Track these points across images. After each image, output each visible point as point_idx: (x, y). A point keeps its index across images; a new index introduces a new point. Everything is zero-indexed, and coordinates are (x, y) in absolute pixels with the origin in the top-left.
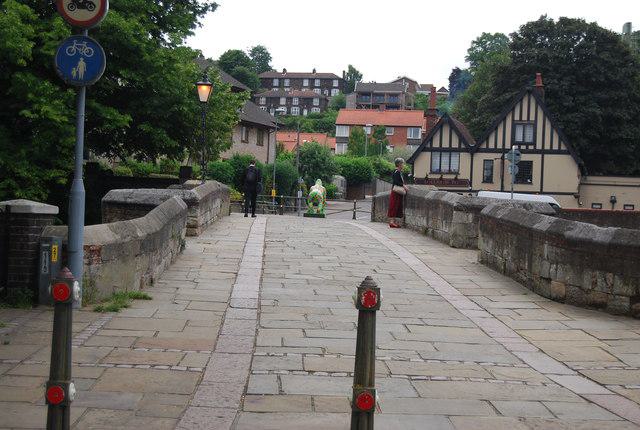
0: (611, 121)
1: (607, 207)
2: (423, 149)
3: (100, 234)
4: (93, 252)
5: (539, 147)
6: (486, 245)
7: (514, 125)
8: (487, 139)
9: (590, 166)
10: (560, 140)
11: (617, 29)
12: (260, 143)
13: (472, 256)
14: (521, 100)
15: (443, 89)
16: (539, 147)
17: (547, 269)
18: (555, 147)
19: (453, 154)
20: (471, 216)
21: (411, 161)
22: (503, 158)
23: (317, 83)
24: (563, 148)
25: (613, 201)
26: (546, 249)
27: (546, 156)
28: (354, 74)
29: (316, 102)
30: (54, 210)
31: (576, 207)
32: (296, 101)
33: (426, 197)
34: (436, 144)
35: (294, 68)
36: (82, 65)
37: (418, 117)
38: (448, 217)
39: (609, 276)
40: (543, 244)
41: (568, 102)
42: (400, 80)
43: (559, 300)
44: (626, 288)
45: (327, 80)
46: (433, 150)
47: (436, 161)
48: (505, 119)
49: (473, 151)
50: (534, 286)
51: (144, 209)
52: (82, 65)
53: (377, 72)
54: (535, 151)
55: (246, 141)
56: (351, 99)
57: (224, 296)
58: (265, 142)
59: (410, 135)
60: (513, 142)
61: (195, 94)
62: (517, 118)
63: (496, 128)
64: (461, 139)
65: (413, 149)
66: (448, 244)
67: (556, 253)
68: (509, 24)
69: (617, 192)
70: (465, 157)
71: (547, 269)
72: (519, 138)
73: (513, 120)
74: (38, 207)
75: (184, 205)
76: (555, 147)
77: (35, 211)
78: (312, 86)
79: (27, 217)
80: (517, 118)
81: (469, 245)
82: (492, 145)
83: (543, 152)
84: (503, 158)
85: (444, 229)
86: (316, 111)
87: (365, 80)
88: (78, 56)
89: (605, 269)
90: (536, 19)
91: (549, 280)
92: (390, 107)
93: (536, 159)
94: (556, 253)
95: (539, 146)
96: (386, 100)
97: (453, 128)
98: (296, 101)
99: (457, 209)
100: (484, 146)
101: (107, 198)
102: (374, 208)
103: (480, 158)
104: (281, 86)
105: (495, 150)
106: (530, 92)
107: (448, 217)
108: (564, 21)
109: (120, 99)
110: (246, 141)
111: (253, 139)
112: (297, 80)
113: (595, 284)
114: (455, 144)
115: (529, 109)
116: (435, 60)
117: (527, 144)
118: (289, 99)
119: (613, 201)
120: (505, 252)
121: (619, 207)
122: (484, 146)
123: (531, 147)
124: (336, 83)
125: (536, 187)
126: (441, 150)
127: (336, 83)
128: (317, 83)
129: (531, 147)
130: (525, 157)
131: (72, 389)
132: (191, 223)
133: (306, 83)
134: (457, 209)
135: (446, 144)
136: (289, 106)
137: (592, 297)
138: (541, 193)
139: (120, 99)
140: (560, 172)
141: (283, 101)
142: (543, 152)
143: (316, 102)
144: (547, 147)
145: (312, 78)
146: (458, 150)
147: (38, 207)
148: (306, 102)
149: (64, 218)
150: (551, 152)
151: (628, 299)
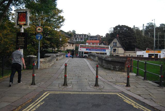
0: (130, 42)
1: (128, 56)
3: (42, 60)
4: (41, 62)
5: (117, 46)
11: (132, 27)
12: (73, 46)
14: (114, 39)
15: (105, 37)
16: (117, 46)
17: (104, 64)
18: (120, 46)
23: (83, 36)
29: (83, 39)
30: (36, 57)
31: (124, 56)
32: (80, 39)
35: (79, 33)
36: (39, 37)
41: (123, 39)
42: (97, 35)
43: (105, 68)
48: (112, 42)
50: (114, 69)
51: (49, 56)
52: (39, 37)
53: (93, 34)
54: (116, 47)
57: (59, 68)
60: (113, 46)
61: (59, 39)
62: (114, 42)
68: (123, 25)
69: (130, 54)
71: (104, 64)
72: (114, 45)
74: (34, 56)
75: (55, 56)
76: (120, 46)
77: (33, 57)
78: (83, 36)
79: (32, 58)
80: (114, 42)
83: (118, 47)
86: (83, 41)
88: (39, 36)
89: (110, 64)
90: (118, 25)
92: (95, 40)
93: (117, 48)
96: (95, 39)
98: (80, 39)
101: (45, 55)
104: (77, 36)
106: (116, 38)
108: (122, 26)
109: (48, 39)
112: (80, 35)
113: (109, 66)
115: (115, 40)
116: (103, 31)
118: (79, 39)
119: (129, 55)
121: (130, 56)
124: (86, 36)
125: (117, 53)
127: (86, 36)
131: (35, 75)
133: (81, 36)
138: (118, 54)
139: (48, 39)
141: (78, 39)
142: (118, 47)
143: (83, 39)
144: (119, 46)
145: (82, 35)
147: (34, 56)
148: (82, 39)
149: (37, 58)
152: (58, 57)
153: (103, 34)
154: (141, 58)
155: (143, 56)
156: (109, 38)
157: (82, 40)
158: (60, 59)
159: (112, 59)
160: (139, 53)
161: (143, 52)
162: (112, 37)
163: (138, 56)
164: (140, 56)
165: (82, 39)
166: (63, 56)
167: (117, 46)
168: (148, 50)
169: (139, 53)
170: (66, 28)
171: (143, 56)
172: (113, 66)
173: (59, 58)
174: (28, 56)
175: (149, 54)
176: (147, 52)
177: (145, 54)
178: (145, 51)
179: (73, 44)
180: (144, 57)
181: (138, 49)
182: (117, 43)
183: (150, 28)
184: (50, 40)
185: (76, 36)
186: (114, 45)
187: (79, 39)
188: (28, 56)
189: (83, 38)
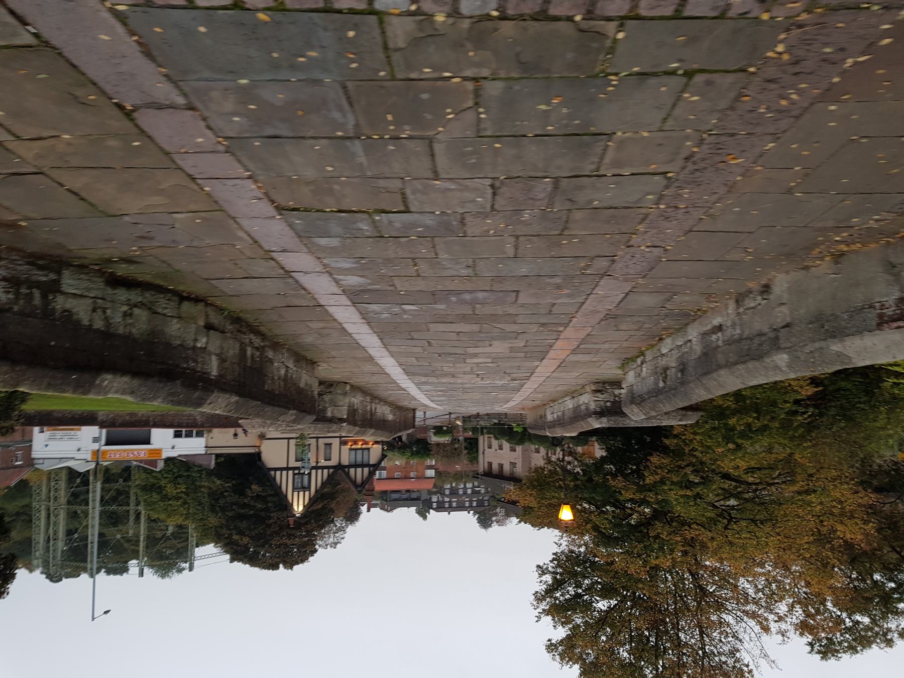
2: (376, 467)
6: (306, 379)
7: (309, 488)
8: (329, 476)
9: (255, 459)
10: (275, 479)
12: (490, 464)
13: (324, 371)
18: (278, 473)
19: (353, 463)
20: (329, 414)
21: (384, 456)
22: (317, 462)
23: (447, 505)
24: (272, 473)
25: (236, 435)
26: (214, 368)
27: (285, 466)
28: (423, 514)
29: (447, 492)
32: (461, 492)
33: (373, 430)
34: (366, 470)
35: (464, 513)
37: (379, 487)
38: (352, 411)
39: (99, 324)
40: (220, 376)
42: (391, 510)
44: (68, 306)
45: (440, 508)
46: (368, 465)
47: (366, 458)
49: (339, 467)
53: (407, 514)
54: (294, 469)
55: (513, 464)
56: (424, 496)
58: (486, 465)
59: (384, 474)
63: (322, 484)
64: (348, 474)
65: (383, 464)
66: (352, 386)
67: (196, 361)
70: (345, 462)
72: (306, 478)
73: (310, 491)
78: (450, 502)
80: (307, 493)
81: (328, 385)
82: (326, 471)
83: (287, 469)
84: (317, 462)
85: (357, 400)
87: (413, 509)
89: (107, 335)
90: (295, 567)
91: (209, 327)
93: (293, 464)
94: (196, 361)
95: (291, 472)
97: (354, 482)
98: (461, 492)
99: (341, 420)
100: (331, 470)
102: (414, 421)
103: (334, 462)
104: (471, 502)
105: (323, 468)
107: (352, 411)
108: (275, 567)
110: (513, 464)
111: (495, 467)
112: (461, 507)
114: (352, 470)
117: (299, 474)
118: (465, 493)
119: (236, 435)
120: (283, 372)
122: (331, 470)
123: (296, 472)
124: (435, 505)
126: (362, 466)
127: (435, 505)
128: (447, 505)
129: (296, 472)
130: (299, 464)
132: (599, 395)
133: (454, 504)
134: (341, 420)
135: (359, 470)
136: (465, 488)
137: (135, 296)
138: (289, 439)
140: (275, 454)
141: (469, 491)
142: (287, 469)
143: (447, 492)
144: (284, 472)
145: (451, 509)
146: (350, 466)
148: (454, 492)
150: (281, 469)
151: (65, 288)
152: (593, 406)
153: (372, 518)
154: (184, 427)
155: (177, 435)
156: (339, 499)
157: (451, 489)
158: (573, 394)
159: (199, 403)
160: (192, 446)
161: (174, 454)
162: (323, 508)
163: (200, 434)
164: (189, 435)
165: (454, 492)
166: (550, 418)
167: (294, 474)
168: (154, 463)
169: (192, 446)
170: (529, 548)
171: (177, 435)
172: (68, 314)
173: (588, 400)
174: (821, 388)
175: (148, 443)
176: (159, 451)
177: (165, 443)
178: (165, 455)
179: (489, 474)
180: (171, 431)
181: (204, 462)
182: (294, 489)
183: (168, 556)
184: (641, 510)
185: (475, 504)
186: (306, 478)
187: (465, 493)
188: (821, 388)
189: (447, 496)
